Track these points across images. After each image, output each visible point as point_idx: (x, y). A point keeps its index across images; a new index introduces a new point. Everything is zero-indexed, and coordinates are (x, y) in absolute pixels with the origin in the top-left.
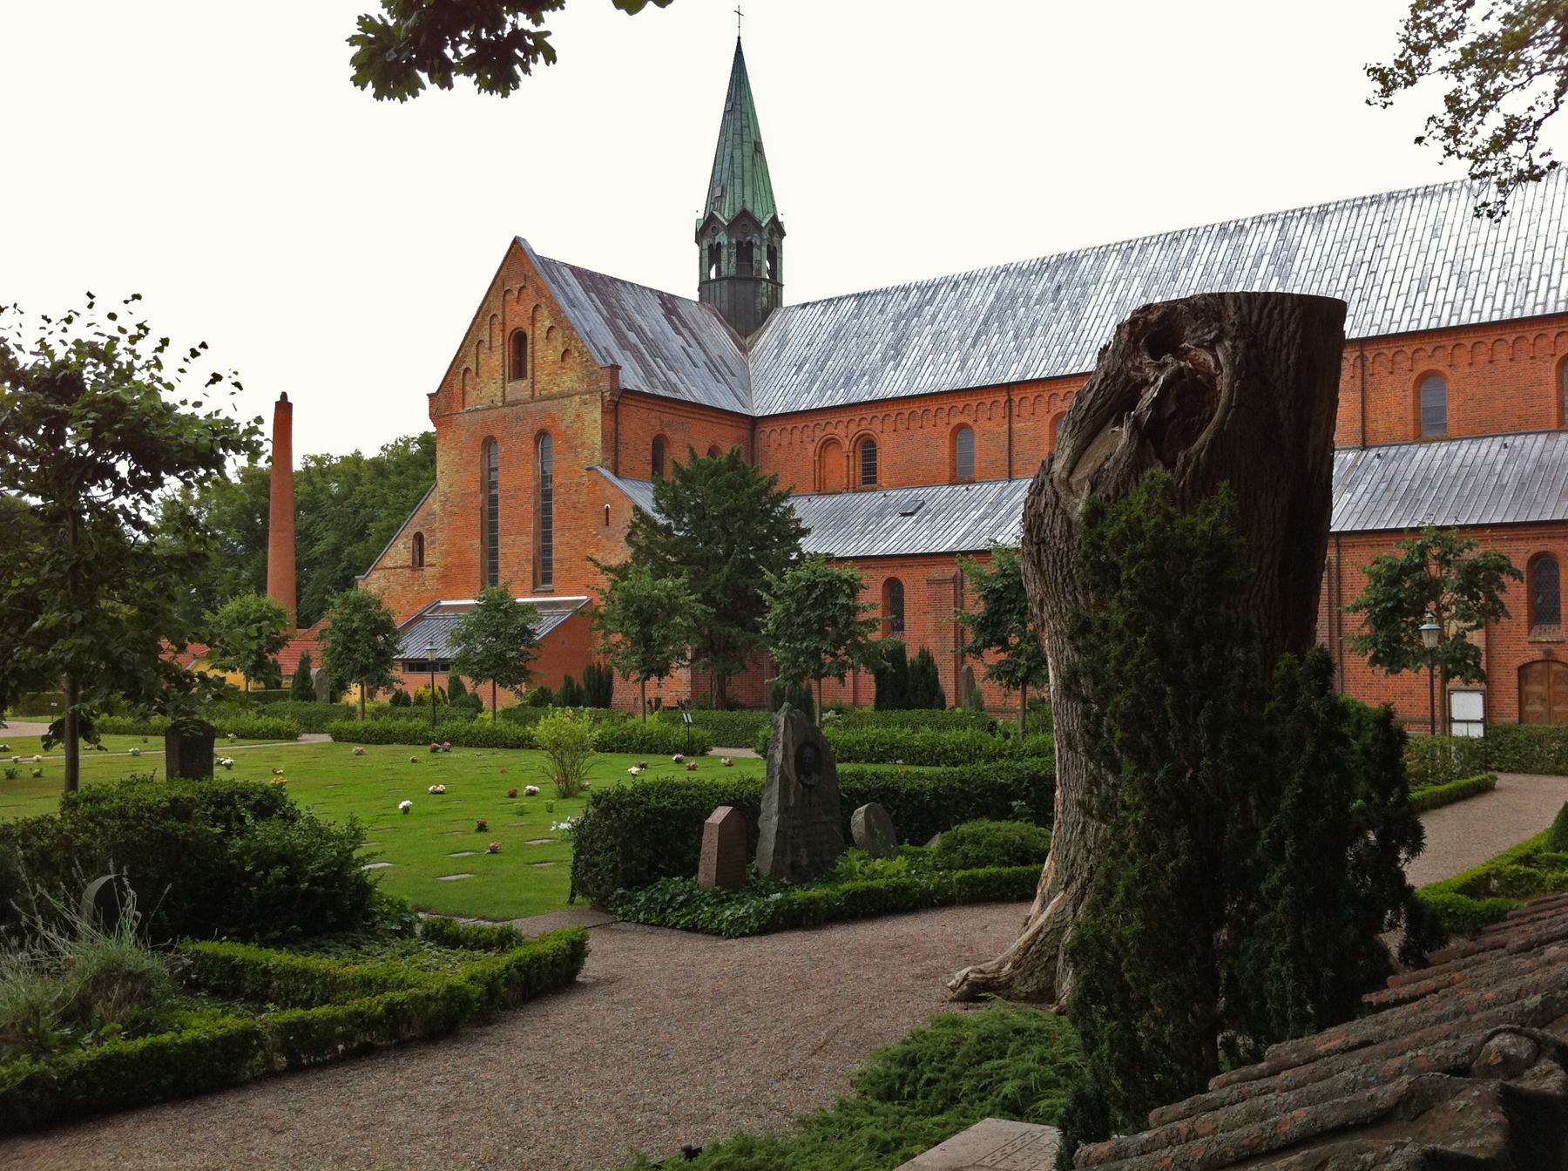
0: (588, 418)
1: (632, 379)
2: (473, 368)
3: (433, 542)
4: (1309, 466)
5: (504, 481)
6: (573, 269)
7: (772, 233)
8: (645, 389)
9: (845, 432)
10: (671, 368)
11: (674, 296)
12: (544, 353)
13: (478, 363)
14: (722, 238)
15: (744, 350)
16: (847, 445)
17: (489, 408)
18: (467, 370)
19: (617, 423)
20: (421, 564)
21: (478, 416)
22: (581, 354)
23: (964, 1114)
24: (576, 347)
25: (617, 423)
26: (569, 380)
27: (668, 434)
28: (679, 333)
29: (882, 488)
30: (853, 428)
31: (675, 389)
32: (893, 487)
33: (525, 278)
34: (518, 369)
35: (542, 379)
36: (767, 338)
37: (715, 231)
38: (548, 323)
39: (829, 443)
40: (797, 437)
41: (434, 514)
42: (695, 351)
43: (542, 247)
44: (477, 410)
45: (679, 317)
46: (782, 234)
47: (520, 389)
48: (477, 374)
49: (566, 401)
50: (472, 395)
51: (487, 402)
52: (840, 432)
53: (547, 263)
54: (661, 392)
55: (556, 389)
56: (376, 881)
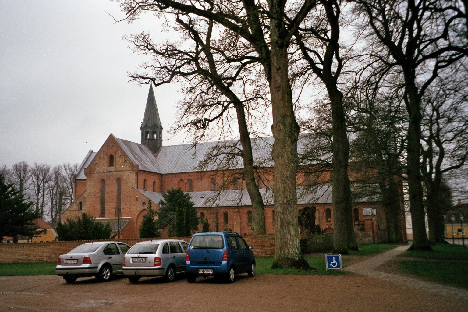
0: (131, 177)
1: (140, 168)
2: (98, 163)
3: (85, 204)
4: (419, 259)
5: (107, 189)
6: (121, 140)
7: (160, 129)
8: (143, 169)
9: (185, 179)
10: (145, 163)
11: (129, 142)
12: (118, 160)
13: (99, 162)
14: (149, 130)
15: (156, 156)
16: (185, 181)
17: (103, 173)
18: (96, 163)
19: (137, 177)
20: (81, 210)
21: (99, 174)
22: (129, 161)
23: (361, 210)
24: (128, 160)
25: (137, 177)
26: (124, 167)
27: (146, 179)
28: (144, 154)
29: (194, 191)
30: (187, 178)
31: (146, 168)
32: (197, 191)
33: (114, 143)
34: (111, 164)
35: (118, 167)
36: (160, 154)
37: (147, 128)
38: (120, 154)
39: (181, 180)
40: (172, 178)
41: (86, 197)
42: (147, 158)
43: (117, 136)
44: (99, 173)
45: (142, 150)
46: (162, 129)
47: (112, 169)
48: (99, 164)
49: (125, 172)
50: (97, 169)
51: (102, 171)
52: (183, 178)
53: (118, 139)
54: (145, 170)
55: (122, 169)
56: (454, 197)
